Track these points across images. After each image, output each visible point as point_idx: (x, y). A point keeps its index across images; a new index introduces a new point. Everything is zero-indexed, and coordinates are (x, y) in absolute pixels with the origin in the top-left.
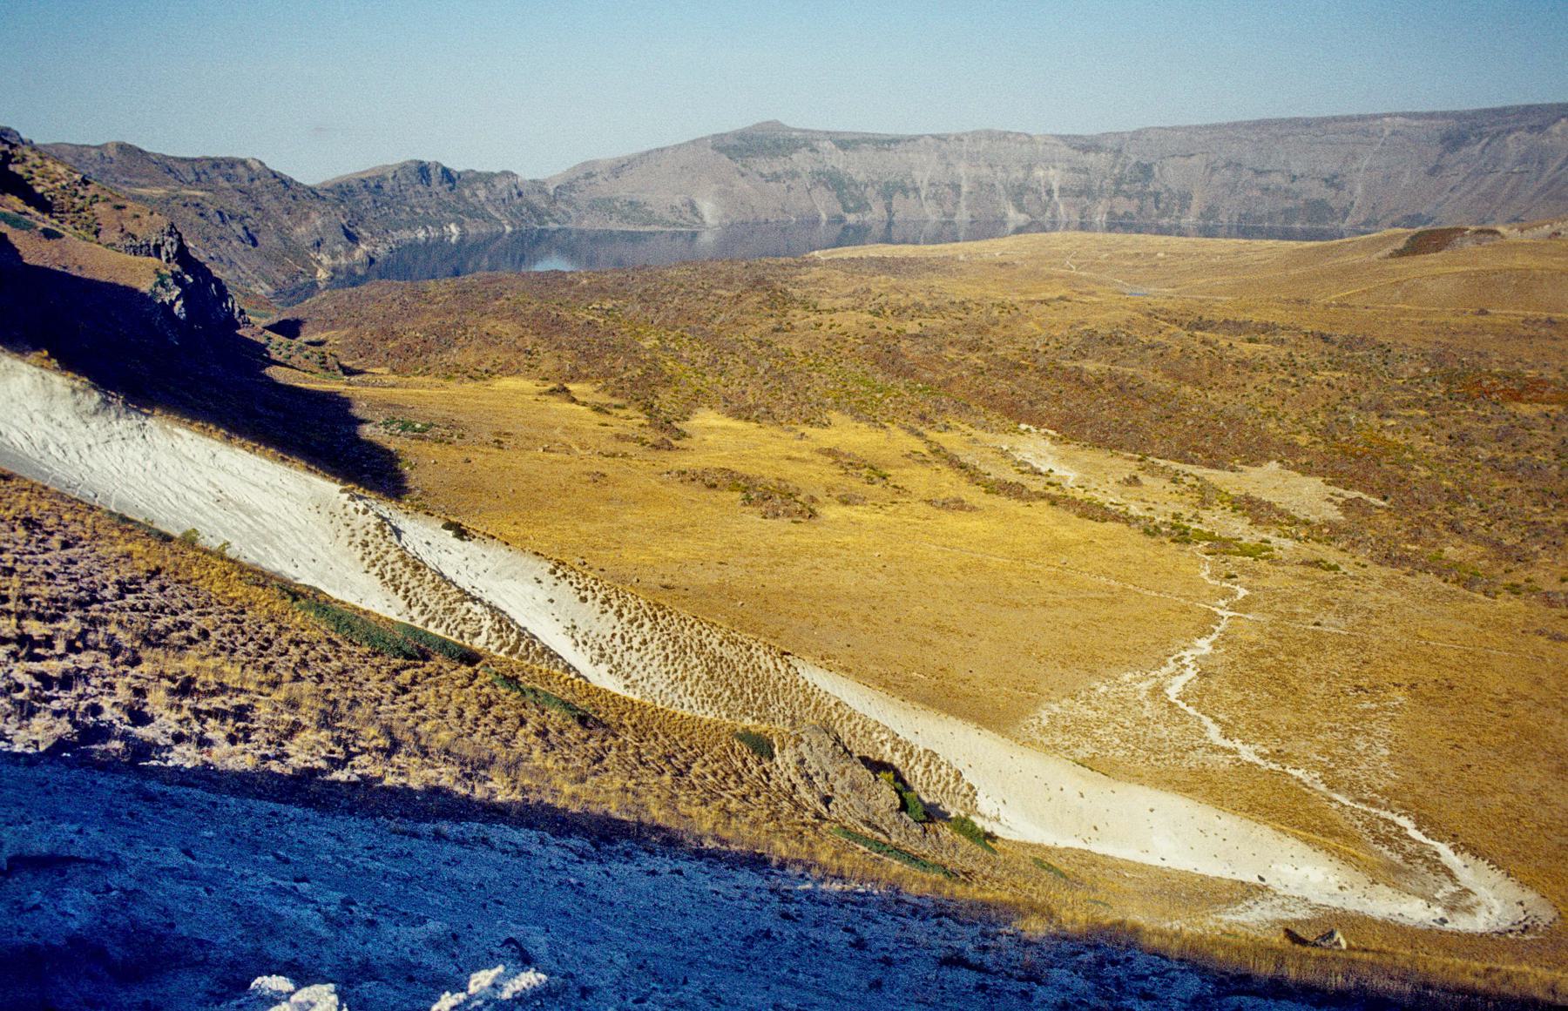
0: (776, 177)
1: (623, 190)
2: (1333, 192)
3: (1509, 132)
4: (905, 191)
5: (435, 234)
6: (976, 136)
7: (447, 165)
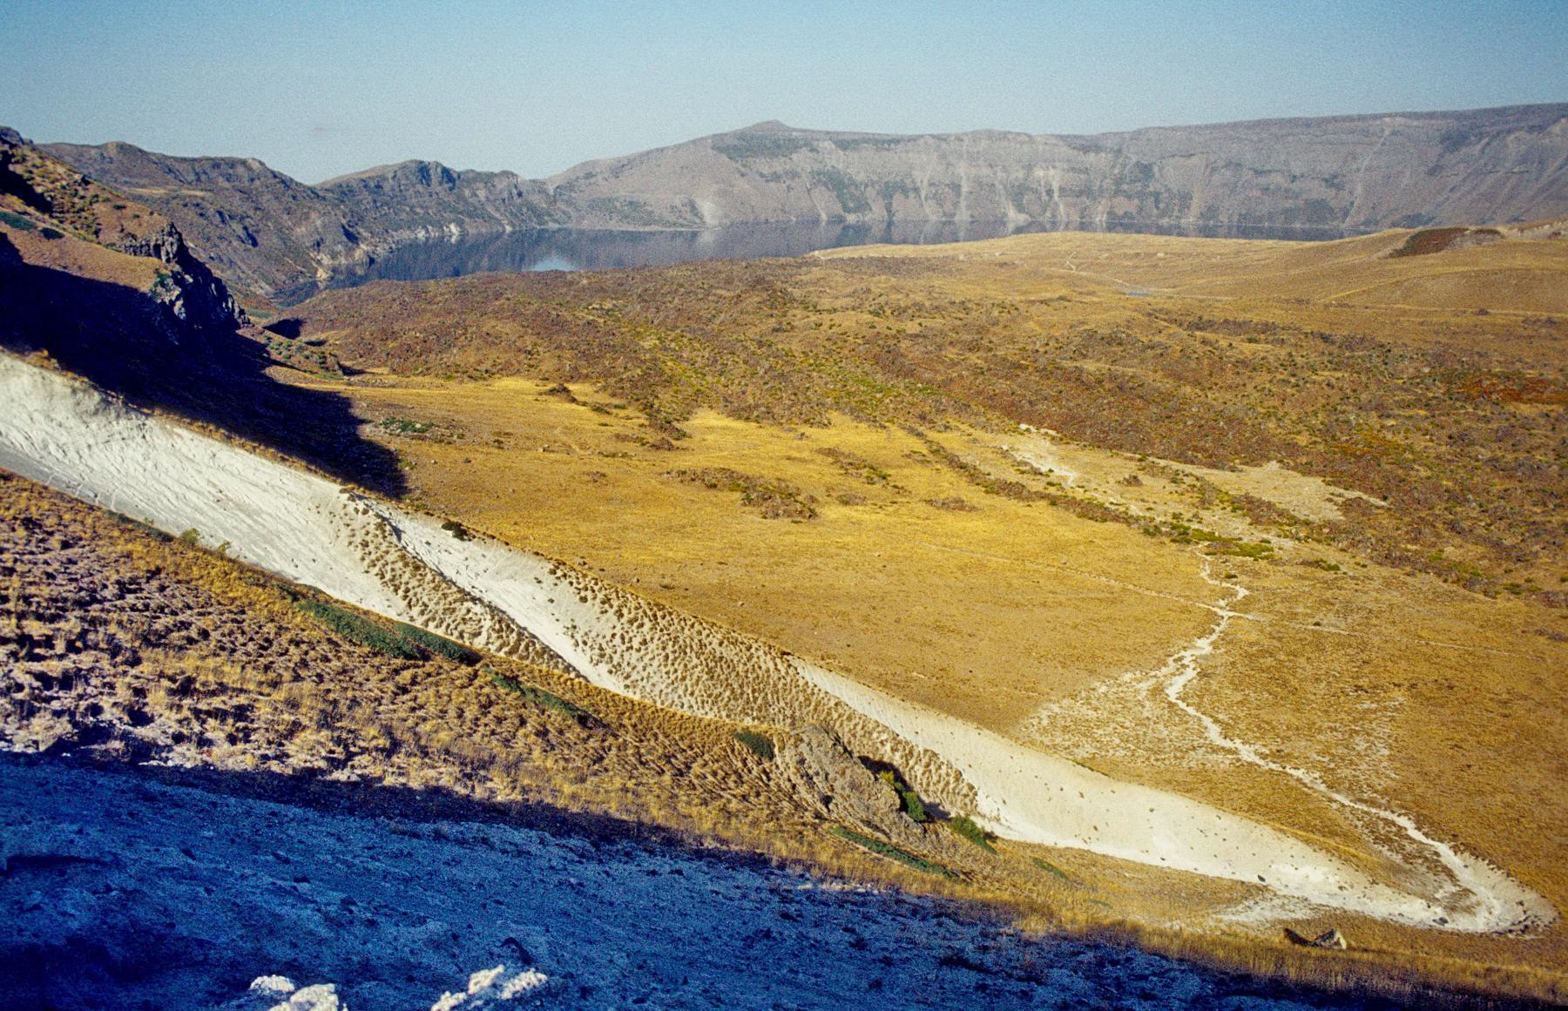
0: (776, 177)
1: (623, 190)
2: (1333, 192)
3: (1509, 132)
4: (905, 191)
5: (435, 234)
6: (976, 136)
7: (447, 165)
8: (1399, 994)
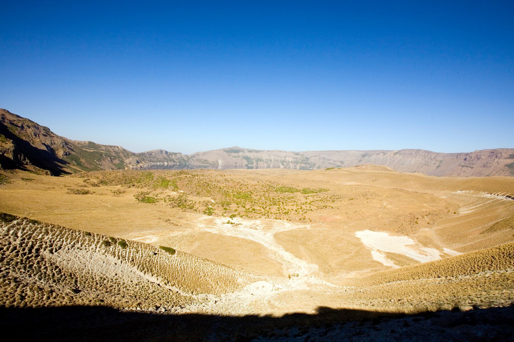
0: (235, 157)
1: (205, 157)
2: (342, 164)
3: (373, 154)
4: (261, 160)
5: (162, 164)
6: (275, 151)
7: (167, 151)
8: (73, 304)
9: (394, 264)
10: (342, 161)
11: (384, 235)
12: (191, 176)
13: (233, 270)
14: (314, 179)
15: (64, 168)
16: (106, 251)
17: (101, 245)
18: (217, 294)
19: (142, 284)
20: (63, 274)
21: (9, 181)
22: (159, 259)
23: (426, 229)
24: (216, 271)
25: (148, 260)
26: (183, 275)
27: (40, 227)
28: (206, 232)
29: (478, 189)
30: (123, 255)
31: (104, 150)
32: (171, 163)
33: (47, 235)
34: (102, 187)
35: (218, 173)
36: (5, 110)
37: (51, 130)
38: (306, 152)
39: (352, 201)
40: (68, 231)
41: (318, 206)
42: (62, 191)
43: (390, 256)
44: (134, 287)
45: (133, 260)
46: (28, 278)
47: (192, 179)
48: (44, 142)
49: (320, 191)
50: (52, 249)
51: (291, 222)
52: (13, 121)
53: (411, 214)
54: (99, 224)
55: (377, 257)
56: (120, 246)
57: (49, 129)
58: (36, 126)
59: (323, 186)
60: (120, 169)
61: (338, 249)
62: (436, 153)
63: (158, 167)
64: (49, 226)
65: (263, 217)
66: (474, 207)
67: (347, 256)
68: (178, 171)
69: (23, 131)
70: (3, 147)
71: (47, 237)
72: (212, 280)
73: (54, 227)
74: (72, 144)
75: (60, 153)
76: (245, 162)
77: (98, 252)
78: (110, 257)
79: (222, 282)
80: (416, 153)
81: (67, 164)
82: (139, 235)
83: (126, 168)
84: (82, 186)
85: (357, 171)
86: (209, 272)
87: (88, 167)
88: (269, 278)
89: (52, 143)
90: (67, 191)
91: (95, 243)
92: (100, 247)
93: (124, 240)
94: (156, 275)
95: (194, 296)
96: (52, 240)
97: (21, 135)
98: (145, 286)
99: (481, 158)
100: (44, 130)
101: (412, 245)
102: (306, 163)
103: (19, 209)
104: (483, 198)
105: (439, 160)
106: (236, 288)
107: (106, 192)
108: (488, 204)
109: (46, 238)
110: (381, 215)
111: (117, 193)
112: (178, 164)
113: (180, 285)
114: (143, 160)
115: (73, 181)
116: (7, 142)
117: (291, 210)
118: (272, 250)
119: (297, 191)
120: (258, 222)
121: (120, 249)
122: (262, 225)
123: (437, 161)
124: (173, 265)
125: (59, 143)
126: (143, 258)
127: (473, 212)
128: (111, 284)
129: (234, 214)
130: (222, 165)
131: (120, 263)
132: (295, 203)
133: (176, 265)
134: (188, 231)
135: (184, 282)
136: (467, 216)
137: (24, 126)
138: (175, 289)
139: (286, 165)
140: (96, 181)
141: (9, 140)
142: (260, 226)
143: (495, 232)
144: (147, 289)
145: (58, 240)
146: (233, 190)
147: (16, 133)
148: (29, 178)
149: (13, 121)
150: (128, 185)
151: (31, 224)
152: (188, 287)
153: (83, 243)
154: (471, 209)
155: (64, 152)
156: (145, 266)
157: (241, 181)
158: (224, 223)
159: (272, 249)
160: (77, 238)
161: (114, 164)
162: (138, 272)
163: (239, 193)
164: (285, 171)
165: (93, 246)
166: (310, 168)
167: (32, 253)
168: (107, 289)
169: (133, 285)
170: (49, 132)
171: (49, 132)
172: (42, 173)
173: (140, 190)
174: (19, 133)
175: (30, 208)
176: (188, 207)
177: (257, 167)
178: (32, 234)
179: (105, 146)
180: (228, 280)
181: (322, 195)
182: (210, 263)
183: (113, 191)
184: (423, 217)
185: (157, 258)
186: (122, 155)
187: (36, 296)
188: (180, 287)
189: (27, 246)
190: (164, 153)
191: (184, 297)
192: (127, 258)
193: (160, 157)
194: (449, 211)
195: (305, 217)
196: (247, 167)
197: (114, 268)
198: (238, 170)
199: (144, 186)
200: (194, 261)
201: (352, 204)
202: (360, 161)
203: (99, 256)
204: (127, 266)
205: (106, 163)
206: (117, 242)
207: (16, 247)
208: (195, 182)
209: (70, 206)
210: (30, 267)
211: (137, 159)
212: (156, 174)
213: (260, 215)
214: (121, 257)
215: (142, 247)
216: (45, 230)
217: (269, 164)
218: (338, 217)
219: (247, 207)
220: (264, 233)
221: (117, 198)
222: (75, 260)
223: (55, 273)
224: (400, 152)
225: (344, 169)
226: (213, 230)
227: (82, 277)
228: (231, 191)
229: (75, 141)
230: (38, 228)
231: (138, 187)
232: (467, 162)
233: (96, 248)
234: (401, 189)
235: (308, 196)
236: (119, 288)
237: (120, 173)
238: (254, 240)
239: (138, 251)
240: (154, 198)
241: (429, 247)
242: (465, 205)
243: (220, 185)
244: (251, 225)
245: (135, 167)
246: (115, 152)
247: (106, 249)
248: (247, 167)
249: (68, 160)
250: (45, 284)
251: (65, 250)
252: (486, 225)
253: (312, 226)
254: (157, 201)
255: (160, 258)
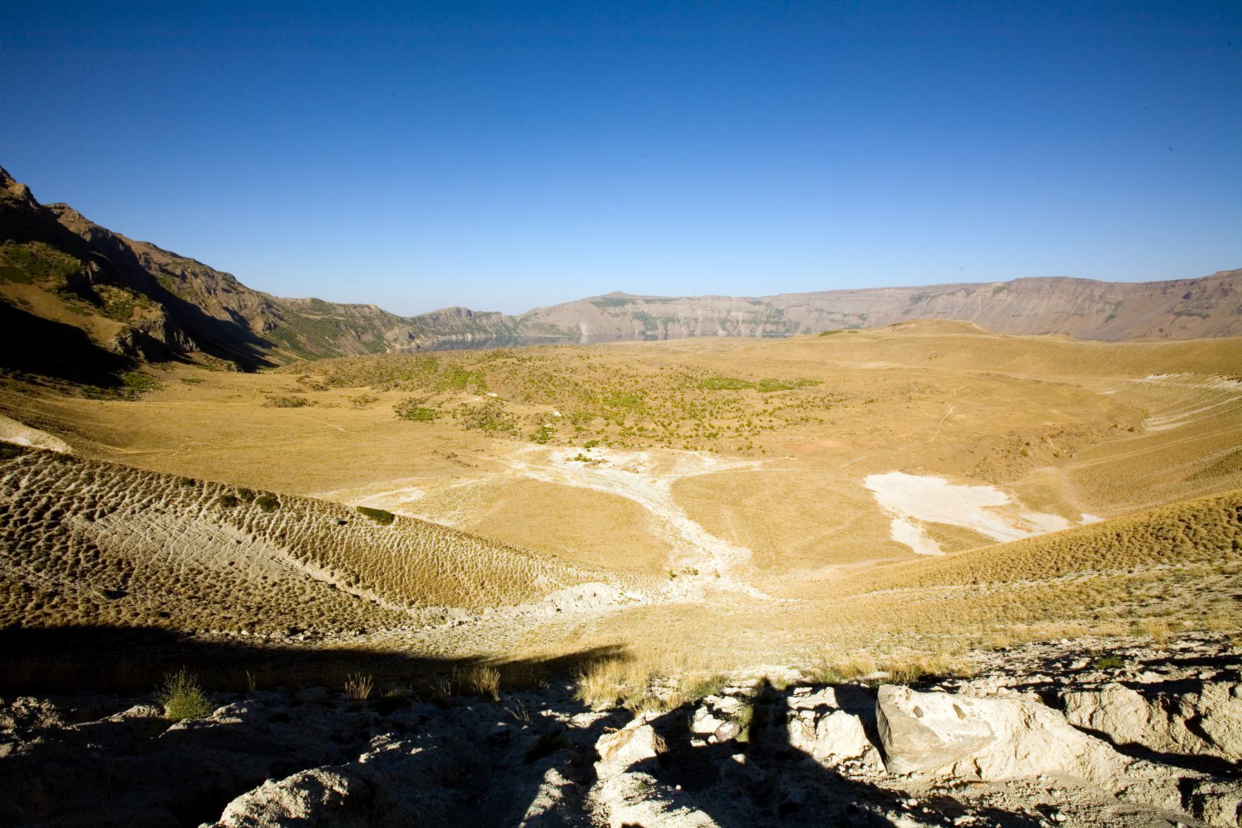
0: (617, 315)
1: (550, 320)
2: (862, 322)
3: (939, 295)
5: (461, 337)
6: (706, 298)
9: (939, 551)
10: (863, 315)
11: (935, 483)
12: (515, 360)
13: (529, 559)
14: (788, 359)
15: (267, 357)
16: (221, 518)
17: (213, 505)
18: (475, 608)
19: (288, 583)
20: (100, 560)
21: (158, 386)
22: (349, 533)
23: (1048, 469)
24: (486, 559)
25: (321, 534)
26: (399, 567)
27: (76, 469)
28: (528, 480)
29: (1204, 369)
30: (261, 524)
31: (342, 316)
32: (480, 336)
33: (89, 485)
34: (334, 391)
35: (575, 352)
36: (149, 244)
37: (239, 280)
38: (776, 298)
39: (870, 406)
40: (142, 477)
41: (789, 419)
42: (255, 401)
43: (936, 531)
44: (266, 589)
45: (283, 536)
46: (11, 568)
47: (517, 367)
48: (225, 305)
49: (800, 385)
50: (93, 513)
51: (718, 456)
52: (165, 266)
53: (1012, 433)
54: (313, 464)
55: (902, 532)
56: (259, 507)
57: (234, 278)
58: (209, 273)
59: (808, 374)
60: (376, 352)
61: (811, 516)
62: (1105, 283)
63: (454, 345)
64: (98, 467)
65: (659, 445)
66: (1187, 415)
67: (829, 531)
68: (490, 352)
69: (185, 285)
70: (145, 318)
71: (89, 488)
72: (469, 579)
73: (109, 468)
74: (279, 306)
75: (258, 326)
76: (638, 326)
77: (203, 518)
78: (230, 530)
79: (496, 583)
80: (1051, 286)
81: (273, 348)
82: (387, 487)
83: (388, 351)
84: (294, 390)
85: (896, 335)
86: (467, 562)
87: (314, 351)
88: (614, 576)
89: (241, 307)
90: (264, 400)
91: (200, 500)
92: (208, 509)
93: (274, 495)
94: (331, 565)
95: (412, 612)
96: (99, 494)
97: (182, 292)
98: (296, 587)
99: (1232, 290)
100: (224, 279)
101: (1000, 507)
102: (776, 323)
103: (171, 439)
104: (1216, 392)
105: (1113, 301)
106: (527, 597)
107: (339, 402)
108: (1227, 405)
109: (85, 489)
110: (935, 437)
111: (360, 403)
112: (495, 336)
113: (387, 586)
114: (422, 331)
115: (278, 381)
116: (151, 308)
117: (726, 429)
118: (659, 516)
119: (748, 386)
120: (644, 456)
121: (257, 513)
122: (652, 463)
123: (1106, 303)
124: (382, 546)
125: (255, 305)
126: (310, 531)
127: (1183, 426)
128: (214, 582)
129: (596, 439)
130: (589, 335)
131: (251, 540)
132: (740, 413)
133: (389, 546)
134: (489, 478)
135: (399, 582)
136: (1162, 436)
137: (186, 273)
138: (368, 595)
139: (731, 328)
140: (320, 379)
141: (155, 303)
142: (647, 464)
143: (1227, 476)
144: (297, 594)
145: (112, 493)
146: (603, 388)
147: (174, 289)
148: (194, 378)
149: (165, 266)
150: (385, 384)
151: (56, 463)
152: (406, 592)
153: (169, 501)
154: (1179, 421)
155: (265, 323)
156: (309, 547)
157: (623, 367)
158: (568, 459)
159: (660, 514)
160: (159, 490)
161: (364, 344)
162: (290, 559)
163: (617, 395)
164: (728, 343)
165: (195, 507)
166: (787, 334)
167: (43, 519)
168: (196, 592)
169: (265, 585)
170: (234, 283)
171: (234, 283)
172: (221, 368)
173: (408, 395)
174: (179, 289)
175: (192, 437)
176: (500, 427)
177: (666, 335)
178: (53, 483)
179: (344, 306)
180: (512, 578)
181: (802, 394)
182: (473, 542)
183: (353, 399)
184: (1043, 440)
185: (344, 531)
186: (379, 323)
187: (11, 601)
188: (385, 590)
189: (34, 504)
190: (464, 313)
191: (386, 611)
192: (268, 531)
193: (457, 322)
194: (1116, 426)
195: (751, 443)
196: (644, 337)
197: (232, 551)
198: (623, 343)
199: (416, 387)
200: (434, 539)
201: (870, 412)
202: (906, 313)
203: (202, 526)
204: (266, 547)
205: (348, 342)
206: (254, 498)
207: (8, 507)
208: (523, 373)
209: (264, 431)
210: (28, 546)
211: (410, 329)
212: (445, 359)
213: (652, 441)
214: (254, 530)
215: (315, 509)
216: (87, 474)
217: (692, 329)
218: (829, 443)
219: (628, 424)
220: (652, 480)
221: (360, 412)
222: (143, 535)
223: (82, 559)
224: (1009, 285)
225: (865, 332)
226: (543, 474)
227: (147, 567)
228: (599, 390)
229: (284, 299)
230: (71, 470)
231: (405, 389)
232: (1191, 304)
233: (200, 510)
234: (998, 375)
235: (771, 397)
236: (229, 591)
237: (370, 362)
238: (627, 495)
239: (302, 517)
240: (434, 411)
241: (1044, 512)
242: (1164, 411)
243: (576, 378)
244: (628, 463)
245: (406, 347)
246: (364, 317)
247: (222, 512)
248: (644, 337)
249: (273, 340)
250: (45, 580)
251: (124, 514)
252: (1206, 459)
253: (764, 465)
254: (439, 415)
255: (353, 531)
